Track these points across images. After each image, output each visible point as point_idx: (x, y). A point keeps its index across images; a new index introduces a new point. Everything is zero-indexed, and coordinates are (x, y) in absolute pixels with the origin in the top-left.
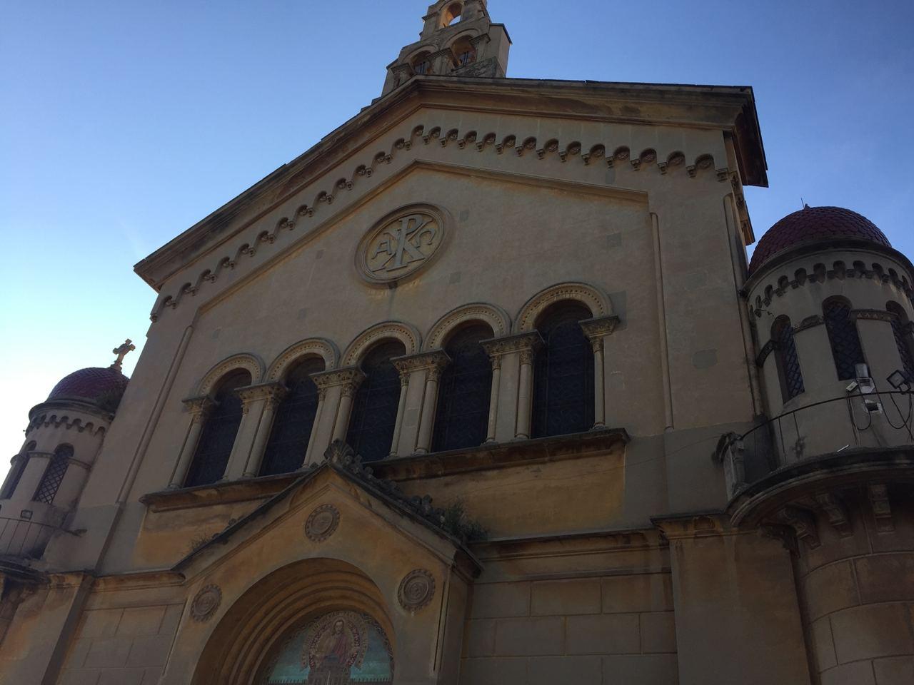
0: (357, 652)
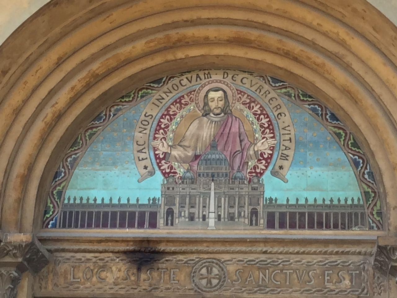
0: (272, 149)
